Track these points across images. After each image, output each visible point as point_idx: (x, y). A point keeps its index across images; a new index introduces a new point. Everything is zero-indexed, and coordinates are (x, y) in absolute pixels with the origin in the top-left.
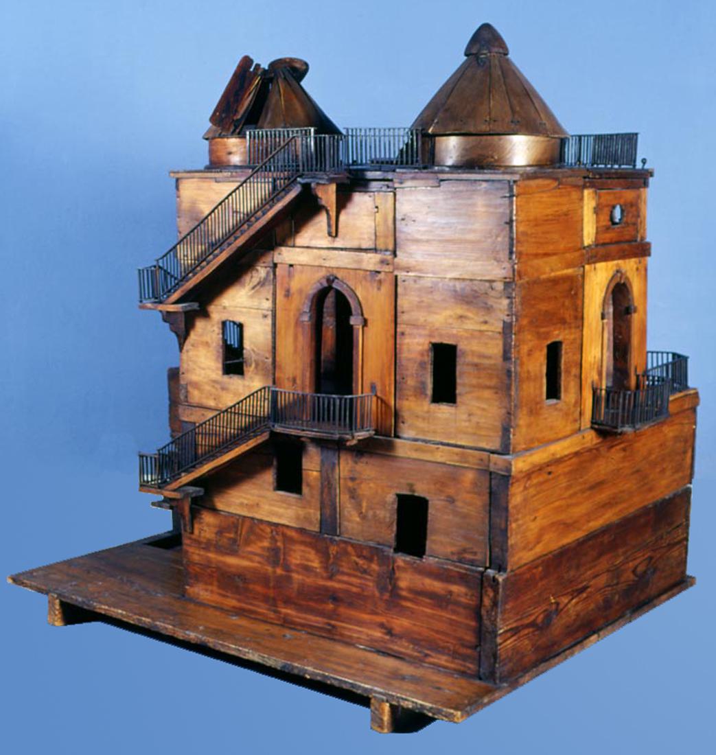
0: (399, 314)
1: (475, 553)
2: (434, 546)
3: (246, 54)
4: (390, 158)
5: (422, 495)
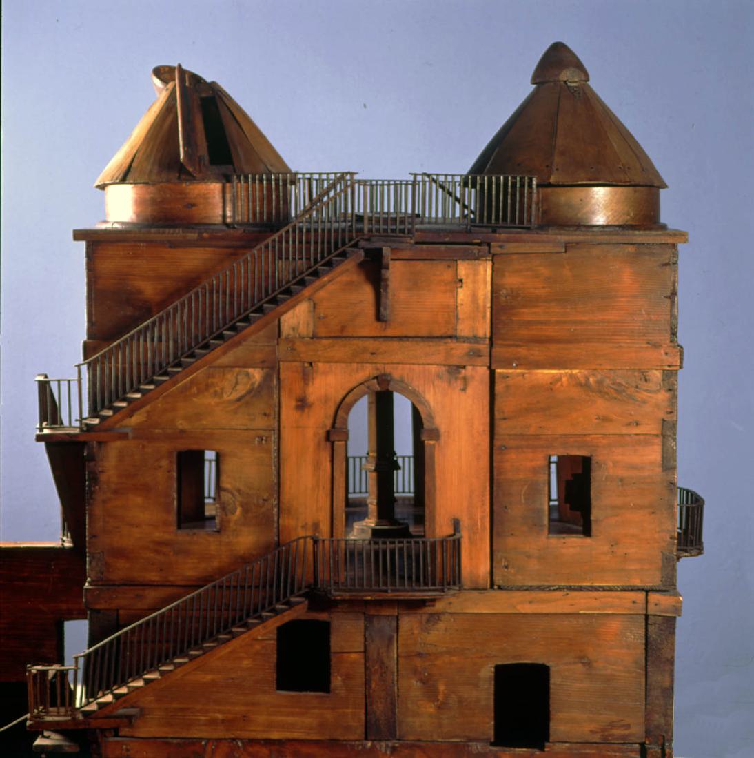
0: (497, 422)
1: (628, 726)
2: (562, 728)
3: (151, 70)
4: (406, 212)
5: (540, 661)
